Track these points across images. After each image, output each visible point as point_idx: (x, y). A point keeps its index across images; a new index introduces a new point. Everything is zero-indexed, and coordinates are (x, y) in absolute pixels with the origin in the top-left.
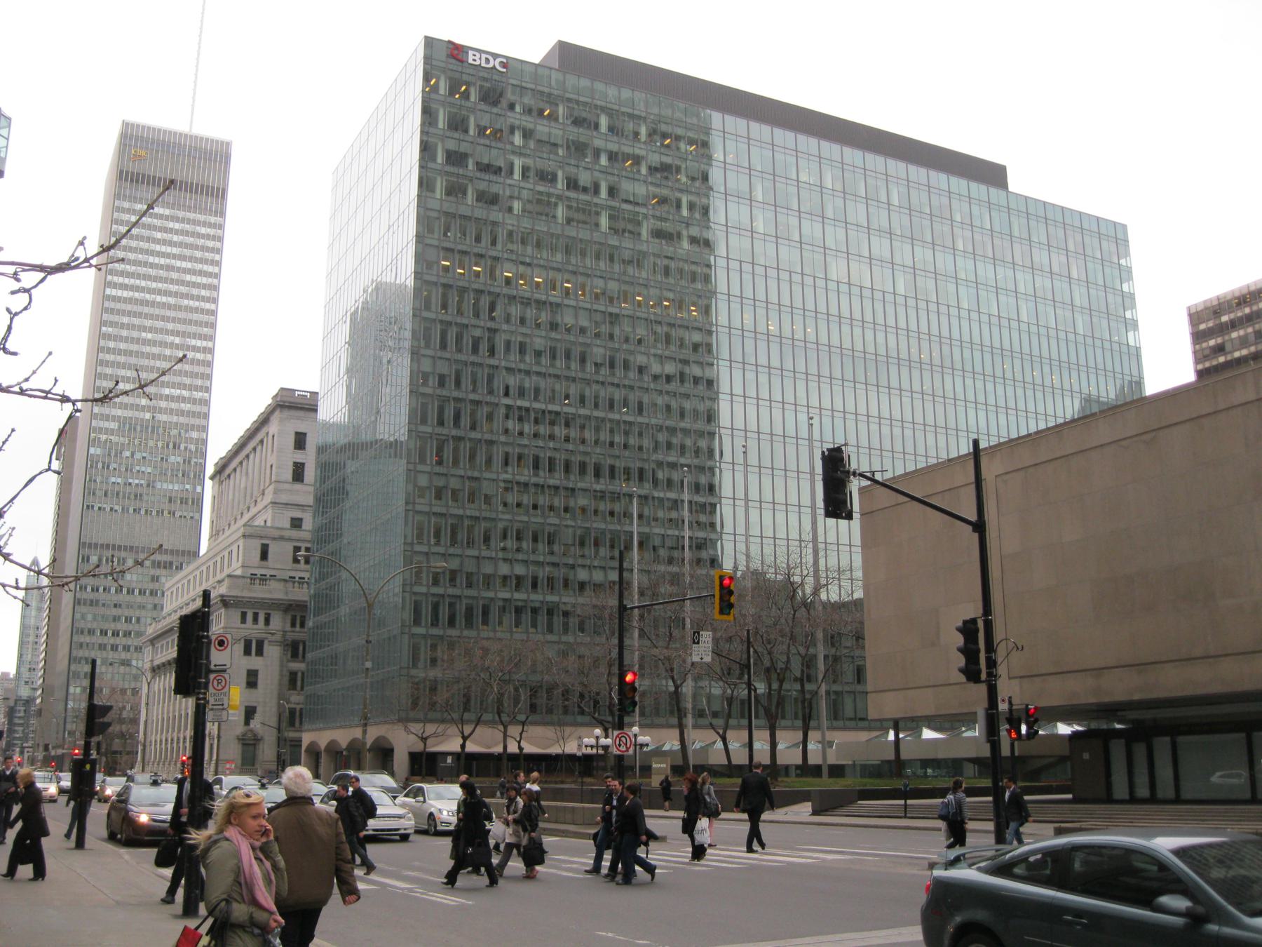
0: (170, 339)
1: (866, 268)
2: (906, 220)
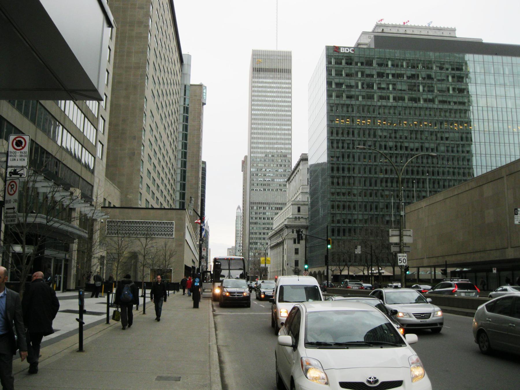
0: (276, 127)
1: (494, 100)
2: (511, 79)
